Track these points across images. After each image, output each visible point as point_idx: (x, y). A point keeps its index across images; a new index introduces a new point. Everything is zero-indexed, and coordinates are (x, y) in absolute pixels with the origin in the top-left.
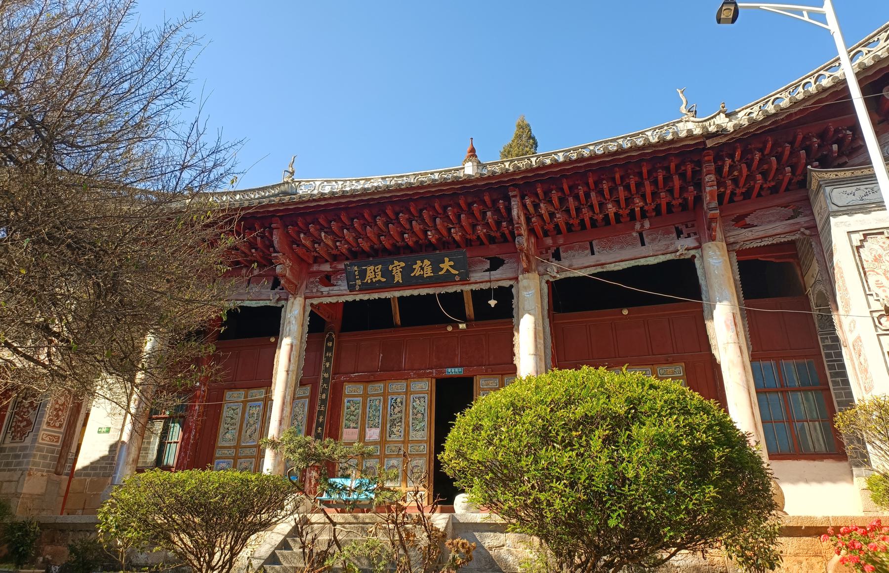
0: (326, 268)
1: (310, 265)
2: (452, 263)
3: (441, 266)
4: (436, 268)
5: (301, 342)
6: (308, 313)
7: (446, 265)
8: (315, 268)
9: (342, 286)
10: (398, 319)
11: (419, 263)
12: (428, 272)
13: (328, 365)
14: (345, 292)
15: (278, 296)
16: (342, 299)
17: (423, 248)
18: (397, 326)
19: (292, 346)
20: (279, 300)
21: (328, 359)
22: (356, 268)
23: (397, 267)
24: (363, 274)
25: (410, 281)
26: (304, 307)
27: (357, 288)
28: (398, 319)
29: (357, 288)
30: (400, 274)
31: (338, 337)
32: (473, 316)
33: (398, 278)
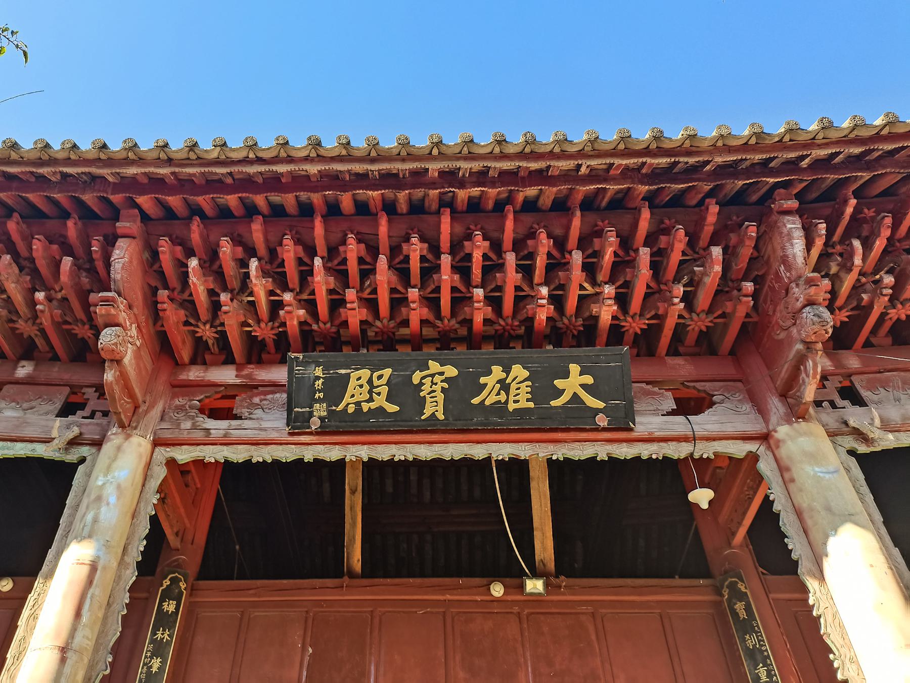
0: (227, 375)
1: (178, 365)
2: (589, 380)
3: (559, 383)
4: (543, 389)
5: (122, 563)
6: (154, 484)
7: (573, 382)
8: (194, 374)
10: (355, 556)
11: (497, 372)
12: (521, 399)
13: (156, 664)
14: (274, 435)
15: (76, 431)
17: (512, 337)
18: (352, 575)
19: (94, 567)
20: (74, 443)
21: (159, 649)
22: (319, 372)
23: (434, 378)
24: (336, 388)
25: (464, 419)
26: (148, 466)
27: (315, 423)
28: (355, 556)
29: (315, 423)
30: (441, 397)
31: (192, 590)
32: (551, 566)
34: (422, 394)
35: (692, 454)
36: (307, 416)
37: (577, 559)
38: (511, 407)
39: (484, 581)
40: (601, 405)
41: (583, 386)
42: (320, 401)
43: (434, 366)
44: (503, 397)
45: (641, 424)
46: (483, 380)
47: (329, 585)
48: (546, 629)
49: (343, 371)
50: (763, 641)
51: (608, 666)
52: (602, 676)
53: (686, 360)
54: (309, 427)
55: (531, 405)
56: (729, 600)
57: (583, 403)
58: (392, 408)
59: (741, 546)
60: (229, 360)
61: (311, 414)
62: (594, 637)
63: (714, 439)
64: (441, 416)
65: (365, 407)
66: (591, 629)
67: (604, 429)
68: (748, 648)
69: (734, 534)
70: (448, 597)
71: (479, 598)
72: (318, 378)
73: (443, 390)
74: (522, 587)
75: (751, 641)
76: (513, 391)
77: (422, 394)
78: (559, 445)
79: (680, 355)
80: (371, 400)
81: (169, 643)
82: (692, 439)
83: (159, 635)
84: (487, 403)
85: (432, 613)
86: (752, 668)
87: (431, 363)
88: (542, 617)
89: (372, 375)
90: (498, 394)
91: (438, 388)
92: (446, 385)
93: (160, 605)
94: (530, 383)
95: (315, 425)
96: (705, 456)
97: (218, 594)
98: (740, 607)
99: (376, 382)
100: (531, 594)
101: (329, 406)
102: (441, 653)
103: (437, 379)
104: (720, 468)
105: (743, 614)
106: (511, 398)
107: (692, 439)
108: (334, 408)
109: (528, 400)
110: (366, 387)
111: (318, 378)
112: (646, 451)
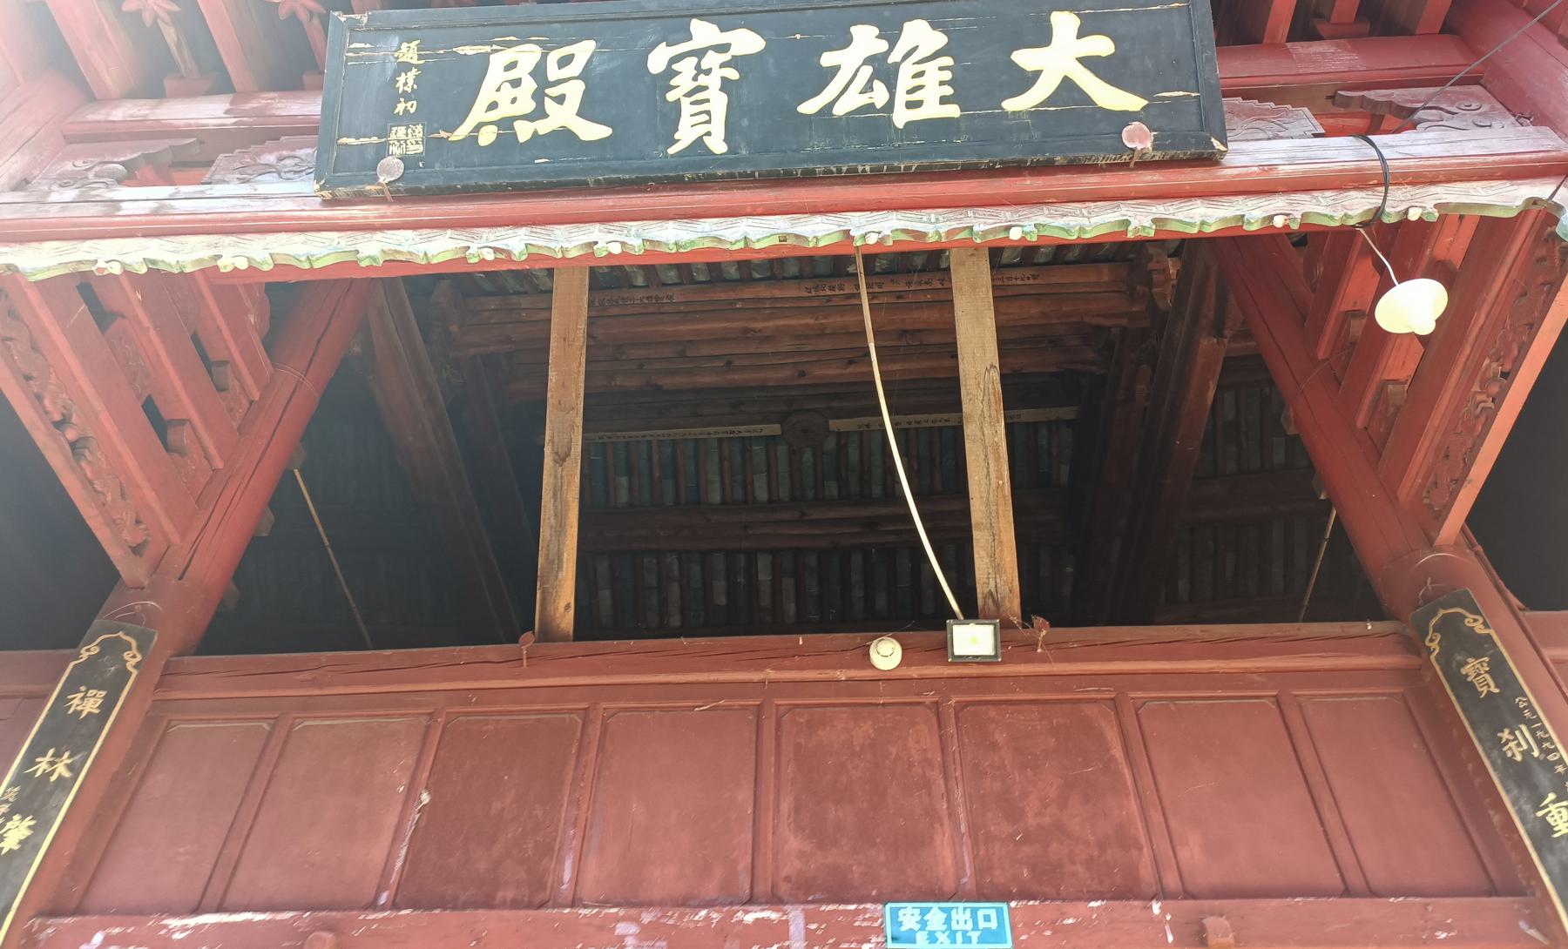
2: (1102, 46)
3: (1025, 58)
4: (983, 73)
9: (290, 190)
10: (560, 596)
11: (866, 39)
12: (926, 92)
16: (261, 252)
18: (548, 635)
24: (451, 89)
28: (560, 596)
29: (390, 170)
30: (719, 103)
32: (1013, 605)
33: (703, 124)
34: (671, 96)
35: (1379, 211)
36: (370, 154)
37: (1077, 581)
38: (901, 117)
39: (857, 638)
40: (1134, 103)
41: (1087, 62)
42: (407, 120)
43: (703, 32)
44: (880, 95)
45: (1238, 152)
46: (827, 59)
47: (490, 657)
48: (1000, 737)
49: (469, 50)
50: (1550, 740)
51: (1157, 817)
52: (1143, 840)
53: (1338, 46)
54: (375, 180)
55: (953, 111)
56: (1446, 658)
57: (1087, 99)
58: (592, 132)
59: (1456, 544)
60: (220, 85)
61: (382, 151)
62: (1118, 753)
63: (1433, 181)
64: (717, 145)
65: (524, 131)
66: (1112, 736)
67: (1146, 165)
68: (1511, 760)
69: (1441, 516)
70: (771, 674)
71: (842, 675)
72: (406, 67)
73: (726, 85)
74: (944, 646)
75: (1518, 744)
76: (905, 81)
77: (671, 96)
78: (1024, 211)
79: (1321, 38)
80: (539, 113)
81: (63, 785)
82: (1385, 179)
83: (42, 765)
84: (839, 110)
85: (728, 708)
86: (1527, 807)
87: (696, 25)
88: (993, 712)
89: (544, 56)
90: (868, 88)
91: (713, 81)
92: (733, 74)
93: (63, 699)
94: (948, 61)
95: (389, 174)
96: (1414, 215)
97: (217, 682)
98: (1475, 669)
99: (553, 73)
100: (964, 660)
101: (428, 131)
102: (744, 796)
103: (712, 60)
104: (1395, 381)
105: (1487, 685)
106: (901, 98)
107: (1385, 179)
108: (443, 134)
109: (944, 100)
110: (529, 85)
111: (406, 67)
112: (1254, 213)
